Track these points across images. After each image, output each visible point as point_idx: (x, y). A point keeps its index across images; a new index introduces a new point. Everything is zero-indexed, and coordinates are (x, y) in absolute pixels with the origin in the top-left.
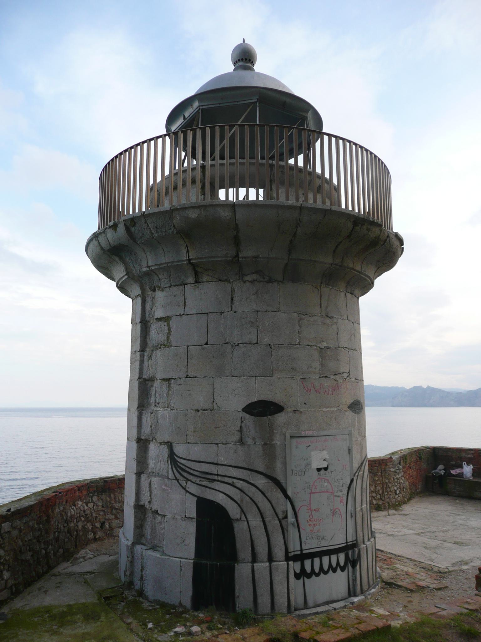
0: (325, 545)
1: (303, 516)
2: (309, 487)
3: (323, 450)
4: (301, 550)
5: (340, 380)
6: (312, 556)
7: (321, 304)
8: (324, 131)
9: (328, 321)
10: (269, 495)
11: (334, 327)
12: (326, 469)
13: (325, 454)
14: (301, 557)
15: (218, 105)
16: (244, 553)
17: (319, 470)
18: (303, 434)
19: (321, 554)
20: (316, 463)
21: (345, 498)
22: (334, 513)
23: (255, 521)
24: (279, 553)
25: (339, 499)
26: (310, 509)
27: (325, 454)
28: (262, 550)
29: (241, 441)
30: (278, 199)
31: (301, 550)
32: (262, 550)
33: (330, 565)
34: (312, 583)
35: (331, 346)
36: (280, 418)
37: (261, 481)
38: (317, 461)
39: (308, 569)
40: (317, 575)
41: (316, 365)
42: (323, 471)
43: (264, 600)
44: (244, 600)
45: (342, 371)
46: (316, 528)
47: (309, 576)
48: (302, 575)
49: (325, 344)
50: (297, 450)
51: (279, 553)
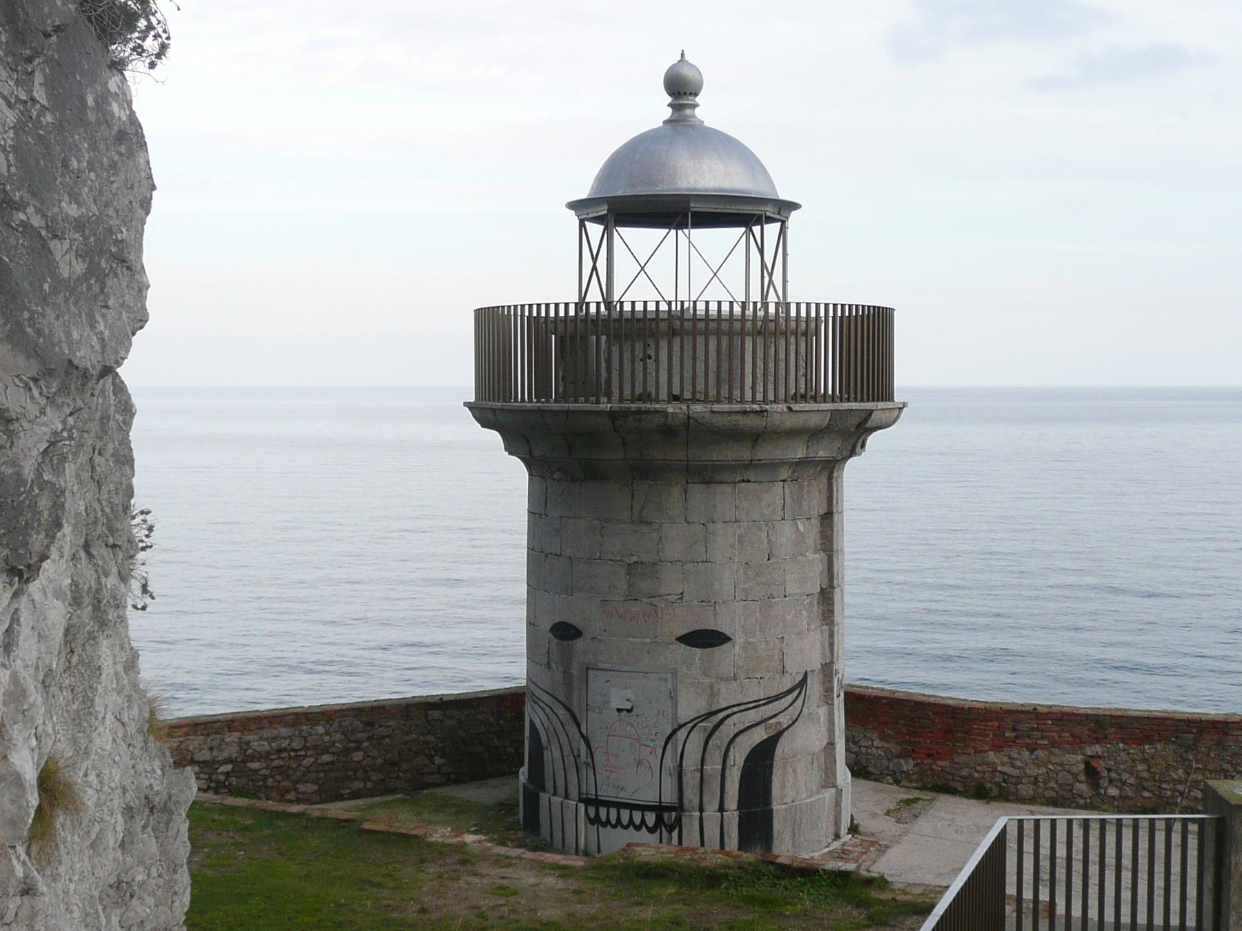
0: (623, 797)
1: (599, 759)
6: (608, 804)
8: (766, 226)
9: (644, 529)
11: (655, 536)
12: (629, 711)
13: (629, 693)
14: (597, 802)
15: (1011, 890)
16: (549, 785)
17: (619, 710)
18: (600, 665)
19: (620, 806)
20: (615, 704)
22: (639, 763)
23: (557, 754)
24: (574, 793)
26: (606, 752)
27: (629, 693)
28: (561, 790)
30: (1070, 822)
33: (631, 821)
36: (579, 644)
37: (562, 712)
41: (622, 586)
43: (558, 835)
46: (613, 776)
47: (604, 825)
49: (635, 559)
50: (597, 681)
51: (574, 793)
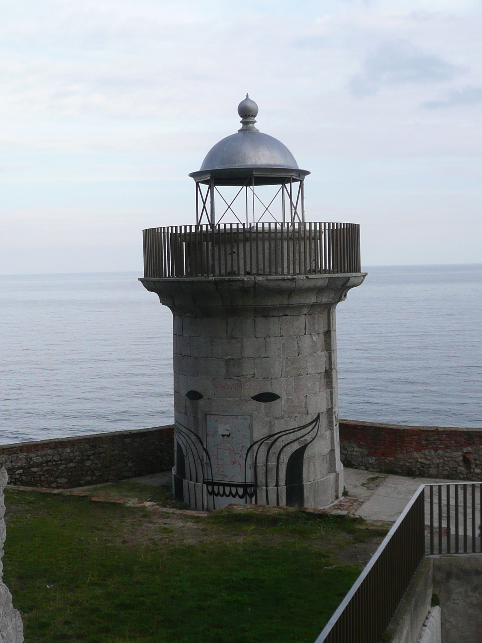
0: (227, 480)
1: (214, 461)
2: (217, 445)
3: (226, 424)
4: (245, 482)
5: (243, 380)
6: (219, 484)
7: (227, 330)
8: (292, 184)
10: (196, 445)
11: (239, 345)
12: (228, 436)
13: (228, 427)
14: (212, 483)
17: (223, 436)
18: (213, 413)
20: (221, 432)
21: (244, 456)
23: (191, 459)
24: (201, 479)
25: (239, 455)
27: (228, 427)
28: (194, 475)
29: (186, 413)
31: (245, 482)
32: (194, 475)
34: (218, 499)
35: (233, 358)
36: (201, 402)
37: (193, 437)
38: (222, 429)
39: (227, 492)
40: (222, 496)
42: (226, 437)
43: (193, 501)
44: (186, 500)
45: (245, 374)
47: (217, 495)
48: (212, 493)
49: (229, 357)
51: (201, 479)
